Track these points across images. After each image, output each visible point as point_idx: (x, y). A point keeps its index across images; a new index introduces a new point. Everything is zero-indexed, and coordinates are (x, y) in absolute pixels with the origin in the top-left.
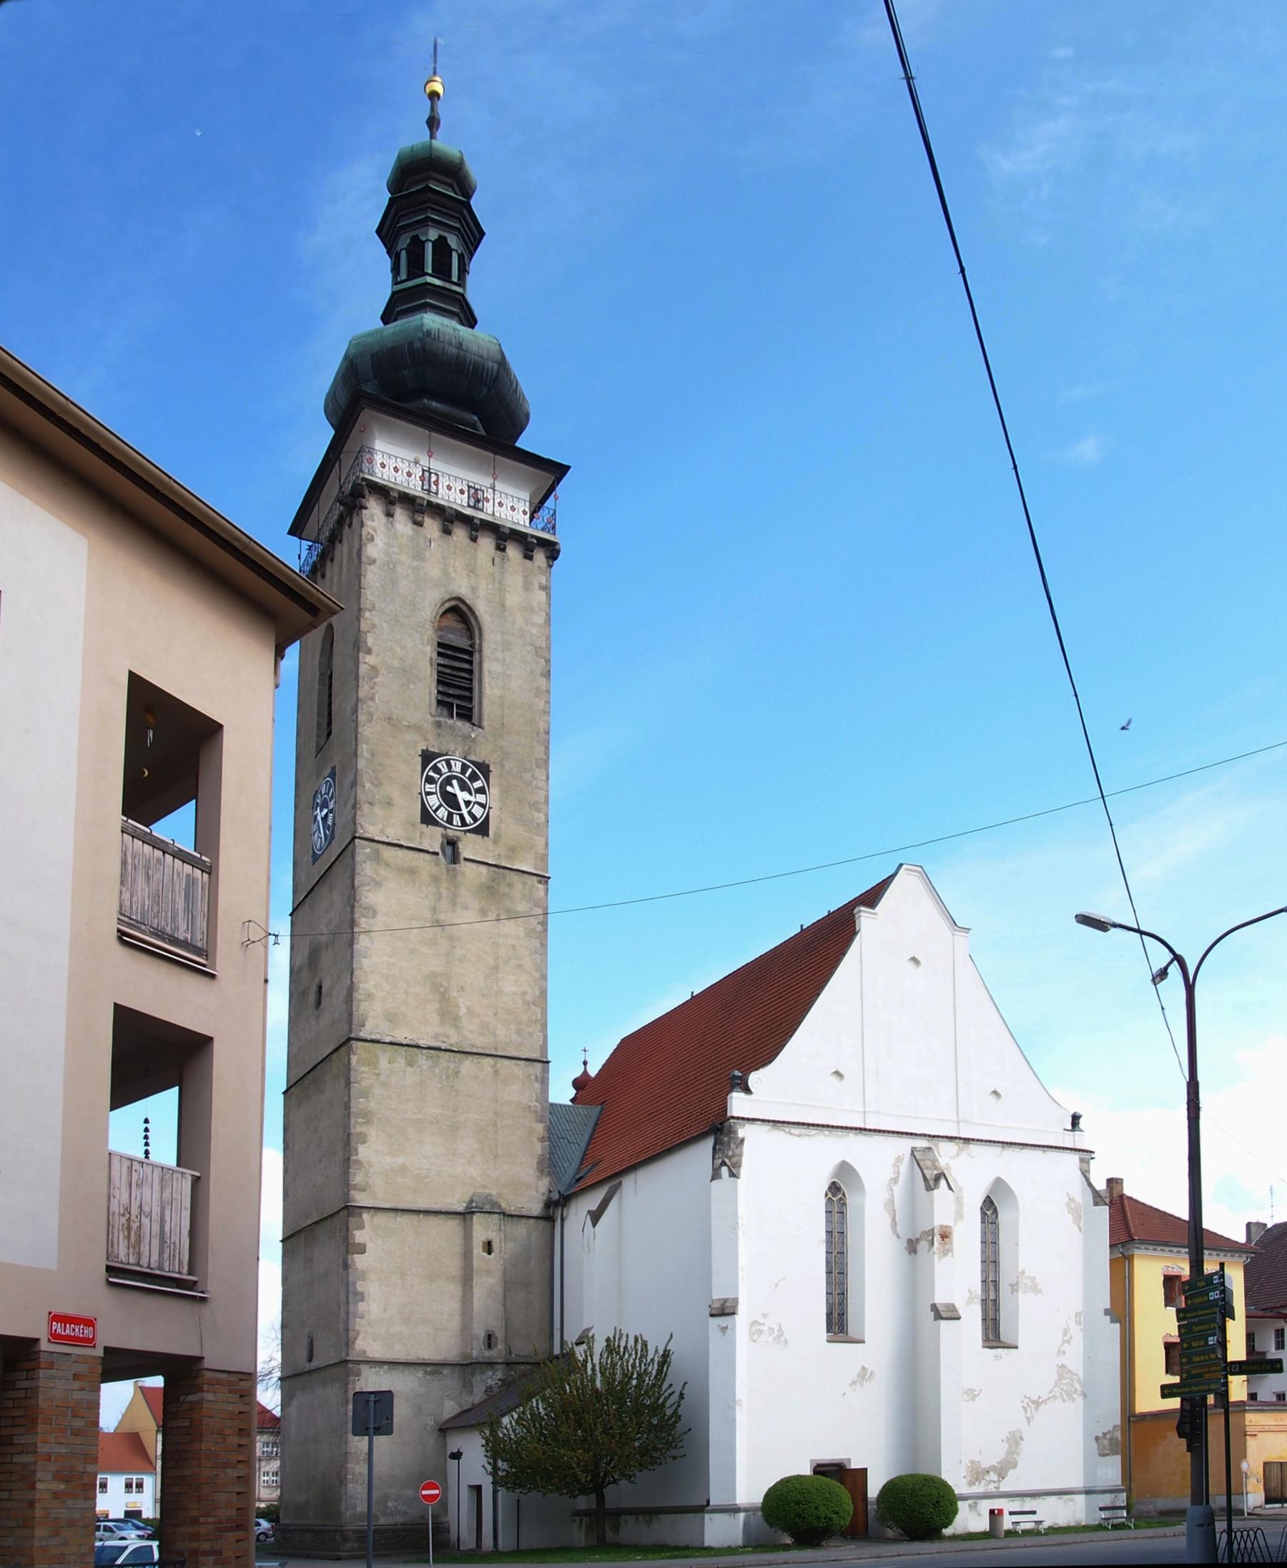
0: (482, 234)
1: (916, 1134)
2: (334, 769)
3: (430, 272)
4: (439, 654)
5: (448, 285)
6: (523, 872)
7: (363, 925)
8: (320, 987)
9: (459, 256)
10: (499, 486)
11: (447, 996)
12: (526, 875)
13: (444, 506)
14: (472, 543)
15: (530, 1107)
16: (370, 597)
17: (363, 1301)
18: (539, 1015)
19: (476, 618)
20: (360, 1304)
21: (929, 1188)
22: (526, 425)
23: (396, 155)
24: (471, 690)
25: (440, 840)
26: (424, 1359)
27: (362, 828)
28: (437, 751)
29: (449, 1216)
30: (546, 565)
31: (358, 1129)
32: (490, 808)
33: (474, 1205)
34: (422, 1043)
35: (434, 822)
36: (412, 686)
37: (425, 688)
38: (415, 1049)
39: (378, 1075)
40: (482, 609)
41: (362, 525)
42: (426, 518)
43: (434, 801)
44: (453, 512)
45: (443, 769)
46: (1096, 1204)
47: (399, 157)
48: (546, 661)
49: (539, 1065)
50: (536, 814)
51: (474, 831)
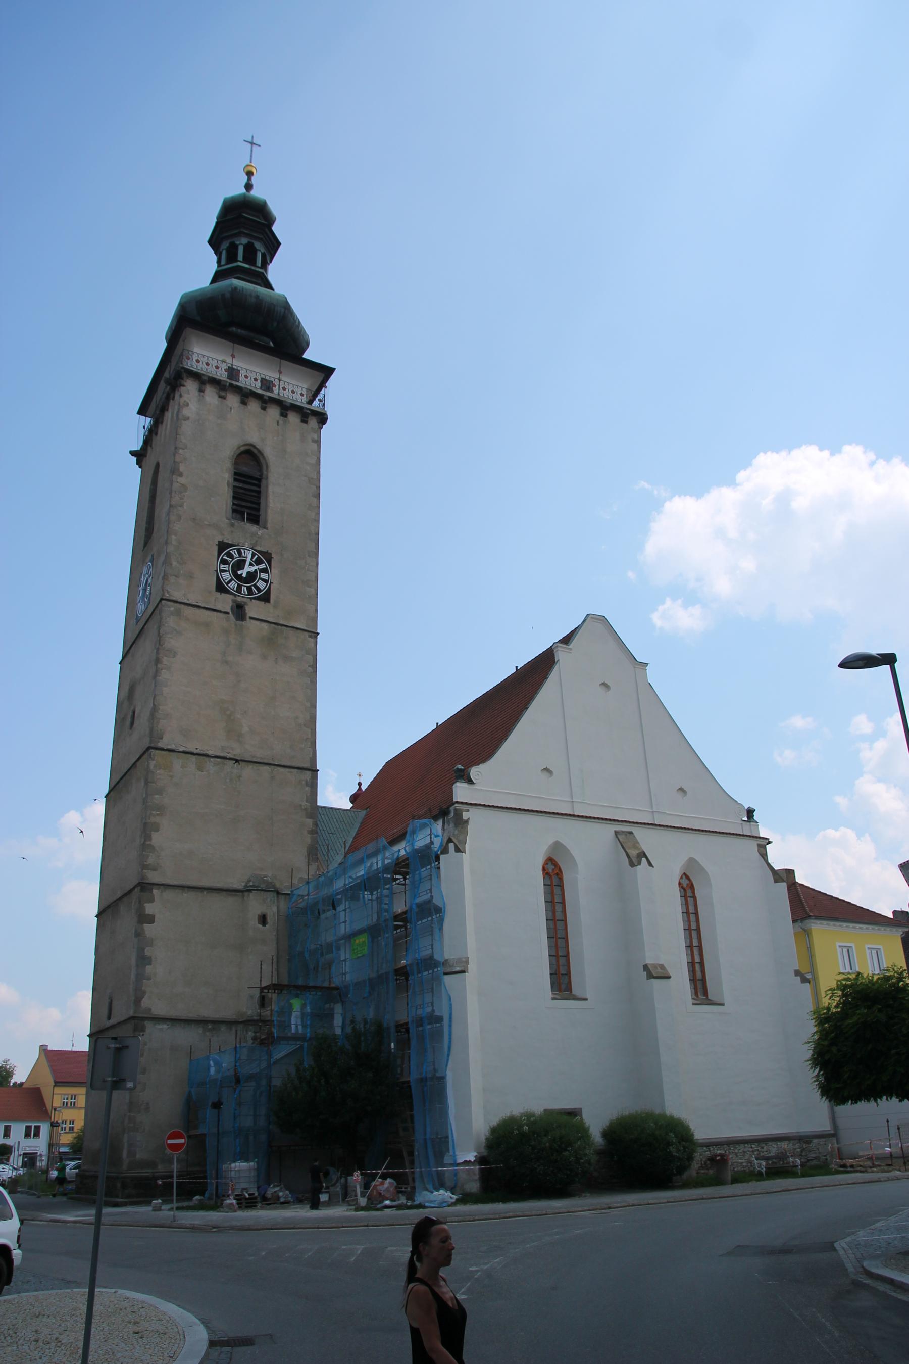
0: (279, 244)
1: (618, 821)
2: (153, 556)
3: (241, 260)
4: (235, 480)
5: (253, 268)
6: (297, 629)
7: (165, 662)
8: (134, 713)
9: (262, 253)
10: (283, 378)
11: (232, 718)
12: (299, 631)
13: (242, 387)
14: (262, 411)
15: (301, 806)
16: (184, 441)
17: (150, 964)
18: (310, 735)
19: (264, 457)
20: (147, 967)
21: (632, 865)
22: (306, 349)
23: (222, 200)
24: (259, 504)
25: (231, 604)
26: (204, 1017)
27: (168, 593)
28: (230, 542)
29: (228, 893)
30: (317, 427)
31: (153, 820)
32: (271, 583)
33: (251, 884)
34: (210, 753)
35: (226, 591)
36: (212, 499)
37: (224, 499)
38: (204, 757)
39: (171, 777)
40: (269, 452)
41: (181, 396)
42: (228, 394)
43: (226, 576)
44: (248, 391)
45: (234, 555)
46: (776, 881)
47: (574, 861)
48: (317, 487)
49: (309, 773)
50: (308, 589)
51: (258, 598)
